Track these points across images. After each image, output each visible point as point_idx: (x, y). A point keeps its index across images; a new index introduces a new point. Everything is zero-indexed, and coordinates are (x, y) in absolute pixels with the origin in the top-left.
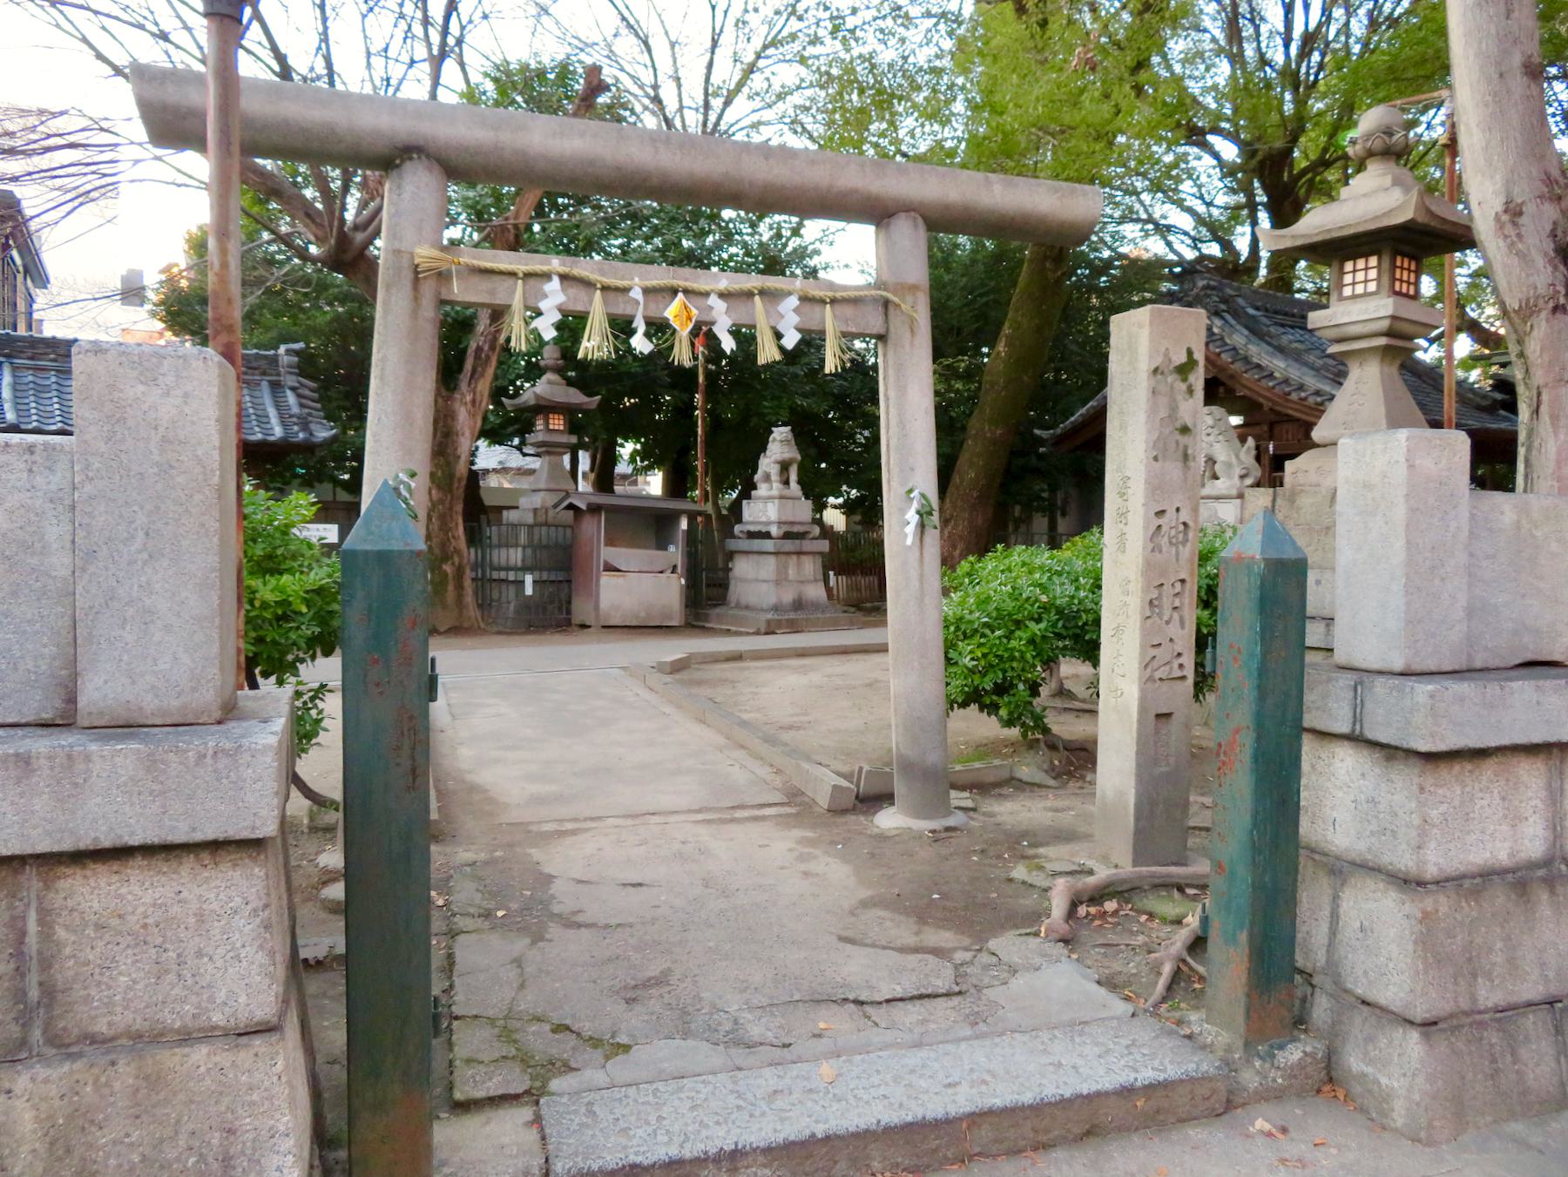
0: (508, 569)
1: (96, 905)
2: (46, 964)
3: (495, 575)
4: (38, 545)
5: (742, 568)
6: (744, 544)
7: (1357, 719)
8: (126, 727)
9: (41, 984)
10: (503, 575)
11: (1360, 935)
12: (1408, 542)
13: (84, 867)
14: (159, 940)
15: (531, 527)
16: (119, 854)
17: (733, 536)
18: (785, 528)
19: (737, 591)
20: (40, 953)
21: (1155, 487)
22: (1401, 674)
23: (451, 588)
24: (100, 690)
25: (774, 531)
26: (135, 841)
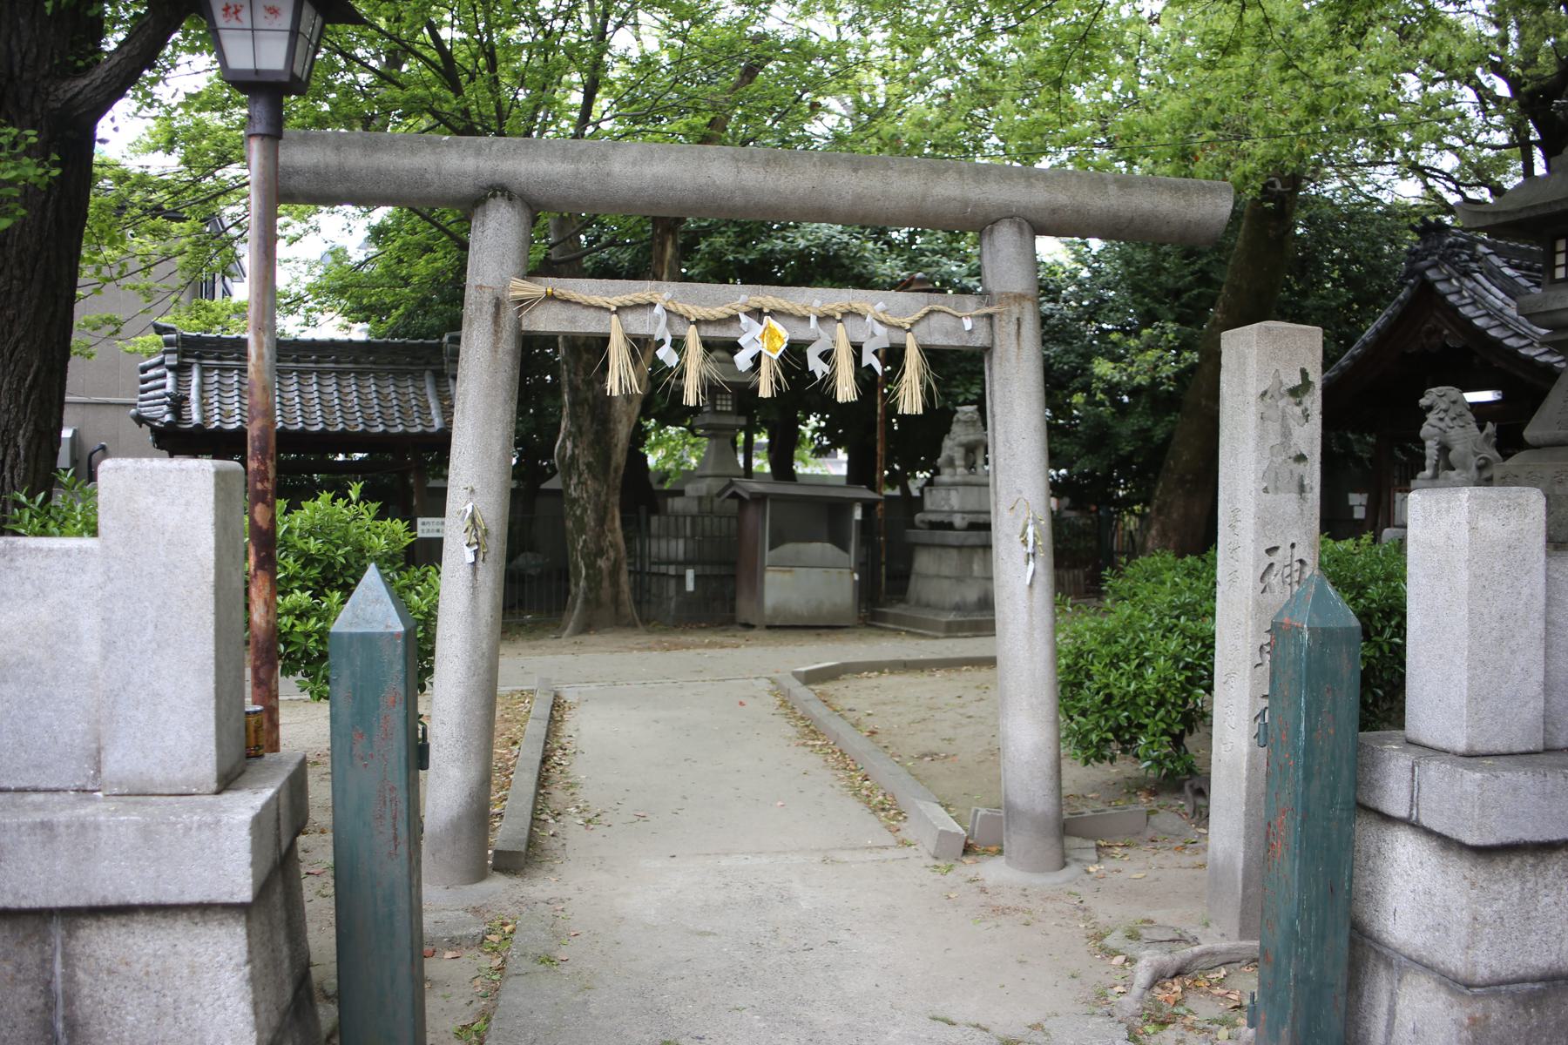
0: (669, 563)
1: (108, 952)
2: (70, 1001)
3: (654, 569)
4: (73, 636)
5: (924, 562)
6: (924, 535)
7: (1413, 802)
8: (140, 793)
9: (65, 1018)
10: (663, 569)
11: (1413, 1038)
12: (1471, 611)
13: (99, 919)
14: (159, 986)
15: (693, 517)
16: (125, 911)
17: (913, 526)
18: (970, 518)
19: (917, 587)
20: (64, 992)
21: (1265, 522)
22: (1463, 756)
23: (606, 584)
24: (120, 762)
25: (958, 520)
26: (136, 899)
